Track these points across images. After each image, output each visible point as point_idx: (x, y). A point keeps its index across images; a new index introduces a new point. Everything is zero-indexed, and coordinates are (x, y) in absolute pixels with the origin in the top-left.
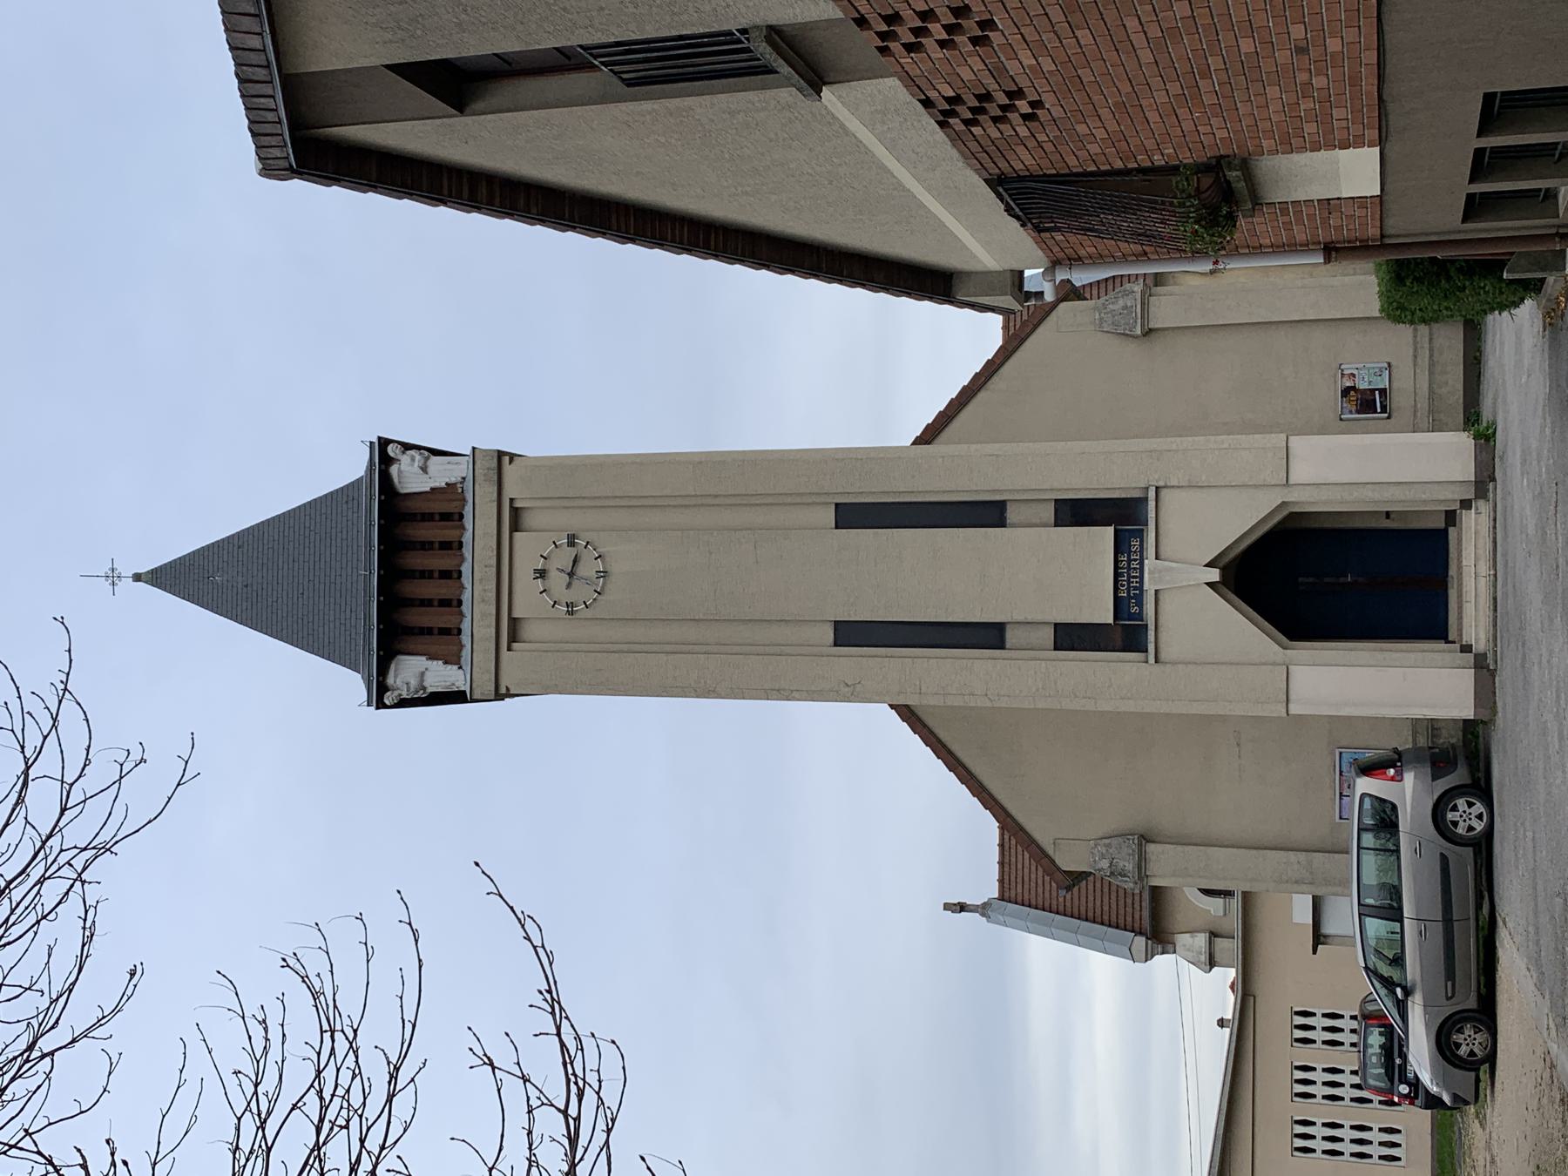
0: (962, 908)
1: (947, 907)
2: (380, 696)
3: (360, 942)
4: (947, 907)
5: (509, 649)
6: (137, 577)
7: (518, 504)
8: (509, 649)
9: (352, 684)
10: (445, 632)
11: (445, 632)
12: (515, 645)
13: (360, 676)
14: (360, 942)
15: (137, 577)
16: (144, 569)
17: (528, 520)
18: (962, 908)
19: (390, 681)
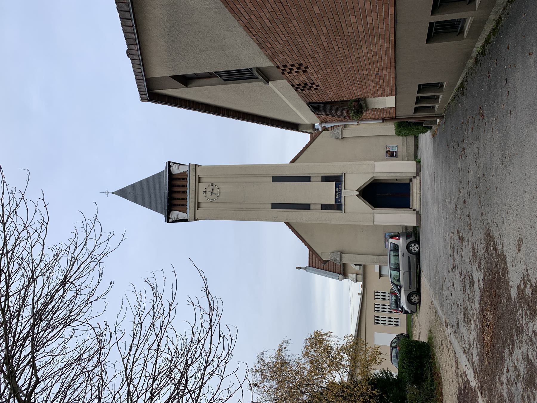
0: (300, 268)
1: (297, 268)
2: (168, 220)
4: (297, 268)
5: (198, 209)
6: (113, 193)
7: (200, 176)
8: (198, 209)
10: (183, 205)
11: (183, 205)
12: (199, 209)
15: (113, 193)
17: (202, 180)
18: (300, 268)
19: (170, 216)
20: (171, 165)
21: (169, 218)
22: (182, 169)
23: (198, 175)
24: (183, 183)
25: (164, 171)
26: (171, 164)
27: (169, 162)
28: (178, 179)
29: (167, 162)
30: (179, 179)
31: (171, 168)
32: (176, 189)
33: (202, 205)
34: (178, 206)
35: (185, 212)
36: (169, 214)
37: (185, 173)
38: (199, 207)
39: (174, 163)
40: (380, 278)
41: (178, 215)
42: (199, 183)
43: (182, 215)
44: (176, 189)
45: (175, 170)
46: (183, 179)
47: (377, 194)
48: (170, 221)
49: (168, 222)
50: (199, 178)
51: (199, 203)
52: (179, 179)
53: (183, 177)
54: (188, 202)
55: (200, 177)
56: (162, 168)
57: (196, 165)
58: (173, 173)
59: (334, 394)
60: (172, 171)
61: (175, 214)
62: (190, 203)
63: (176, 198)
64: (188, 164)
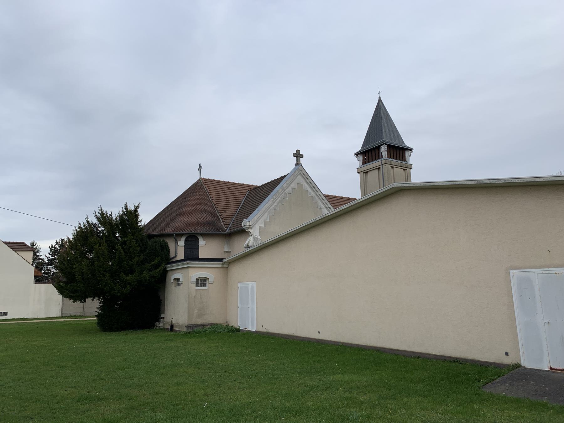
2: (357, 154)
3: (298, 155)
6: (380, 98)
9: (359, 148)
12: (364, 173)
13: (360, 149)
15: (380, 98)
61: (361, 157)
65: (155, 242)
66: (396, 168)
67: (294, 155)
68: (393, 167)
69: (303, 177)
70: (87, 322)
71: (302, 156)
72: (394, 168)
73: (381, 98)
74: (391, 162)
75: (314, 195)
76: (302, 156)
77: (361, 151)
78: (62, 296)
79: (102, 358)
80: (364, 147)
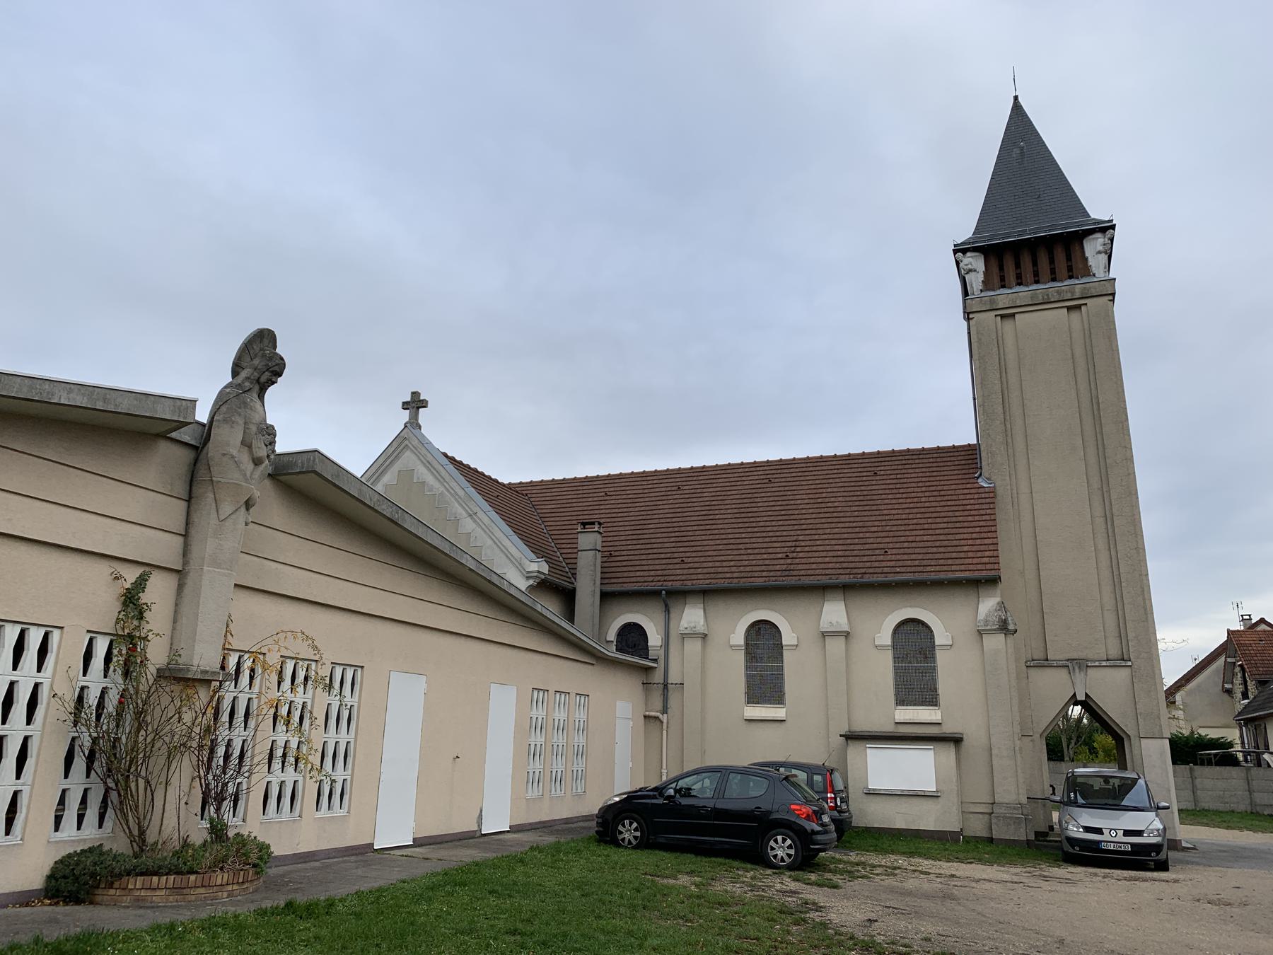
2: (960, 250)
3: (415, 404)
5: (996, 316)
7: (1083, 308)
9: (965, 229)
10: (1002, 279)
11: (1002, 279)
14: (415, 404)
15: (1016, 98)
16: (1020, 99)
17: (1075, 316)
19: (969, 254)
20: (1107, 233)
21: (964, 251)
22: (1095, 260)
23: (1086, 304)
24: (1029, 276)
25: (1086, 214)
26: (1110, 231)
27: (1113, 227)
28: (1053, 258)
29: (1114, 222)
30: (1069, 258)
31: (1099, 235)
32: (1026, 261)
33: (1008, 324)
34: (1067, 256)
35: (987, 285)
36: (975, 249)
37: (1087, 271)
38: (1002, 317)
39: (1112, 240)
40: (841, 736)
41: (975, 271)
42: (1066, 310)
43: (976, 281)
44: (1026, 261)
45: (1092, 247)
46: (1070, 269)
47: (812, 847)
48: (960, 254)
49: (955, 252)
50: (1079, 307)
51: (1013, 315)
52: (1069, 258)
53: (1076, 267)
54: (1027, 289)
55: (1014, 316)
56: (1097, 212)
57: (1113, 294)
58: (1084, 242)
59: (223, 846)
60: (1091, 237)
61: (976, 262)
62: (1004, 297)
63: (1002, 261)
64: (1112, 275)
65: (211, 505)
66: (1022, 315)
67: (405, 405)
68: (1013, 315)
69: (415, 453)
70: (727, 846)
71: (423, 404)
72: (1016, 316)
73: (1019, 99)
74: (992, 302)
75: (442, 489)
76: (423, 404)
77: (973, 243)
78: (268, 422)
79: (72, 926)
80: (979, 233)
